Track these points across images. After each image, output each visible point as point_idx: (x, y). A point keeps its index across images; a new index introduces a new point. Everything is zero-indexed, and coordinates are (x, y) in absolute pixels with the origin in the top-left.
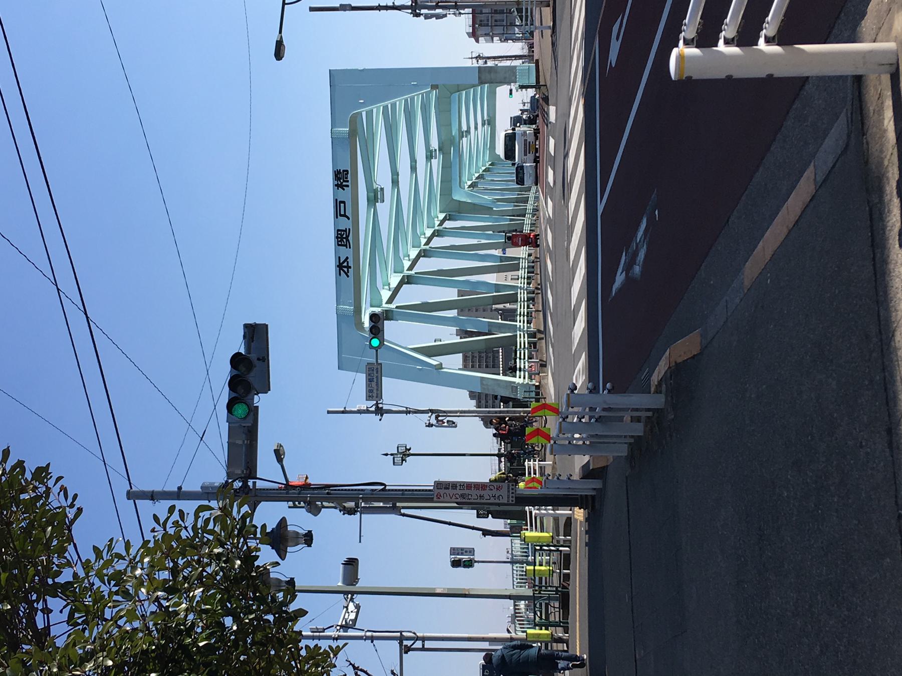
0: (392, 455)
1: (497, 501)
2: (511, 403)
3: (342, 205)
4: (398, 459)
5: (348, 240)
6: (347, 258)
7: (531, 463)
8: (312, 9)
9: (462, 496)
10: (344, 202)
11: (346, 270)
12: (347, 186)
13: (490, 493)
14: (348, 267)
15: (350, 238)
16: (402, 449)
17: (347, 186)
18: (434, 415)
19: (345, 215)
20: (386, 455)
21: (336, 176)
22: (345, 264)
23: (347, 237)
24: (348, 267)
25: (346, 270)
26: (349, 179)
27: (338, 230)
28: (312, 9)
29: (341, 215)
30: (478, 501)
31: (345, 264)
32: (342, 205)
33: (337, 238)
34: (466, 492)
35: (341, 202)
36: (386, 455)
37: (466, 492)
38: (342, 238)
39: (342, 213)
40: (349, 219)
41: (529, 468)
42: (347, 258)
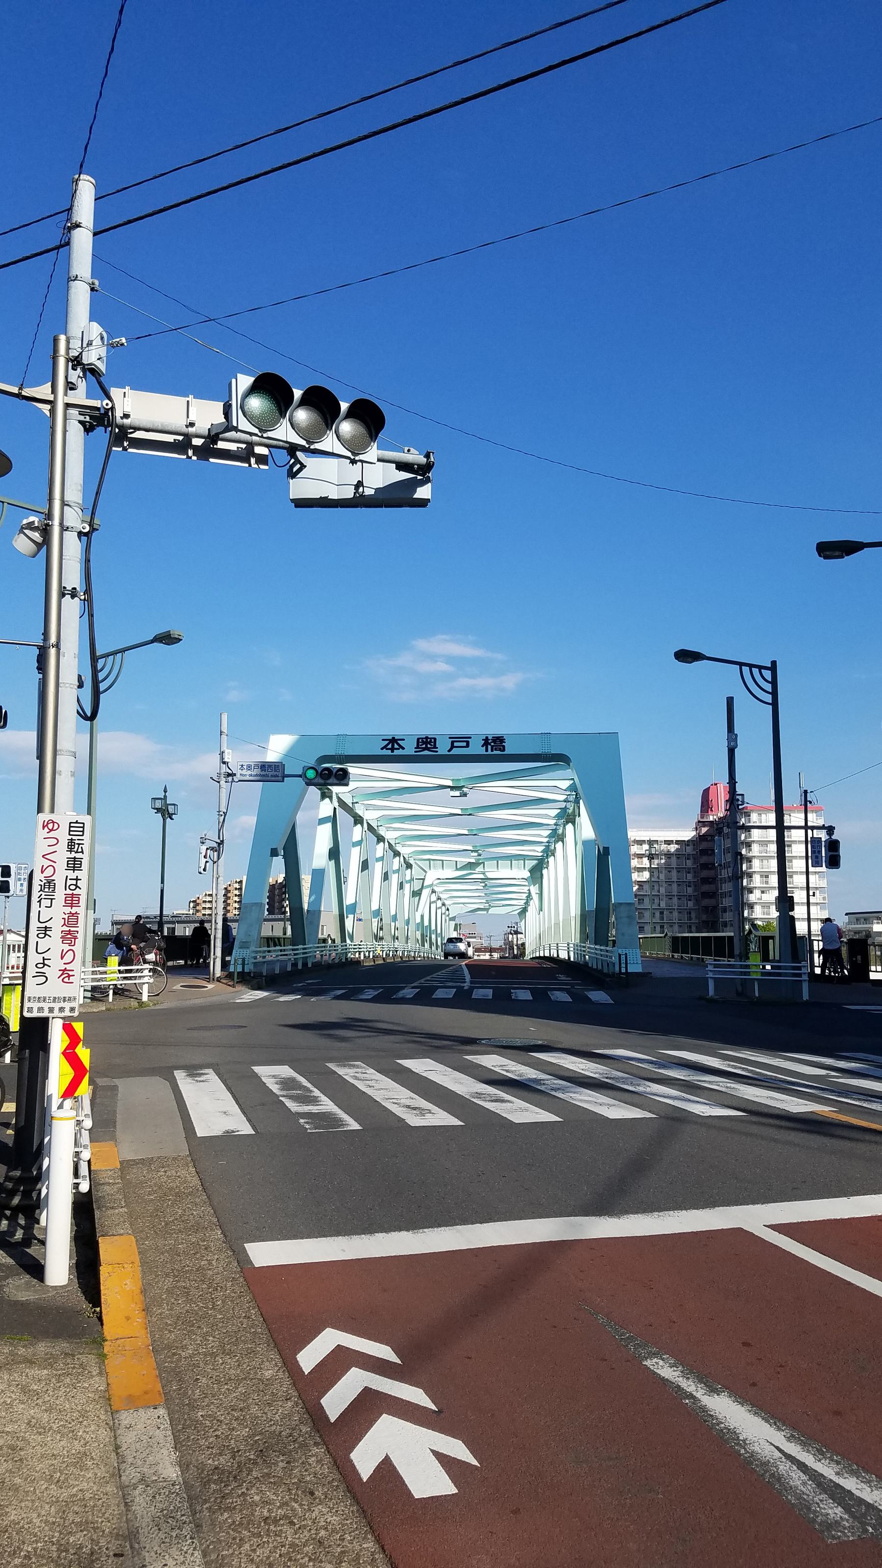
0: (165, 796)
1: (31, 970)
2: (228, 958)
3: (464, 744)
4: (158, 804)
5: (424, 749)
6: (403, 748)
7: (146, 973)
8: (730, 701)
9: (50, 884)
10: (468, 746)
11: (390, 746)
12: (487, 751)
13: (54, 957)
14: (392, 749)
15: (426, 752)
16: (171, 809)
17: (487, 751)
18: (215, 845)
19: (453, 747)
20: (165, 791)
21: (498, 738)
22: (396, 746)
23: (428, 749)
24: (392, 749)
25: (390, 746)
26: (495, 752)
27: (435, 739)
28: (730, 701)
29: (453, 743)
30: (34, 924)
31: (396, 746)
32: (464, 744)
33: (427, 738)
34: (60, 893)
35: (468, 743)
36: (165, 791)
37: (60, 893)
38: (426, 743)
39: (456, 744)
40: (449, 751)
41: (141, 971)
42: (403, 748)
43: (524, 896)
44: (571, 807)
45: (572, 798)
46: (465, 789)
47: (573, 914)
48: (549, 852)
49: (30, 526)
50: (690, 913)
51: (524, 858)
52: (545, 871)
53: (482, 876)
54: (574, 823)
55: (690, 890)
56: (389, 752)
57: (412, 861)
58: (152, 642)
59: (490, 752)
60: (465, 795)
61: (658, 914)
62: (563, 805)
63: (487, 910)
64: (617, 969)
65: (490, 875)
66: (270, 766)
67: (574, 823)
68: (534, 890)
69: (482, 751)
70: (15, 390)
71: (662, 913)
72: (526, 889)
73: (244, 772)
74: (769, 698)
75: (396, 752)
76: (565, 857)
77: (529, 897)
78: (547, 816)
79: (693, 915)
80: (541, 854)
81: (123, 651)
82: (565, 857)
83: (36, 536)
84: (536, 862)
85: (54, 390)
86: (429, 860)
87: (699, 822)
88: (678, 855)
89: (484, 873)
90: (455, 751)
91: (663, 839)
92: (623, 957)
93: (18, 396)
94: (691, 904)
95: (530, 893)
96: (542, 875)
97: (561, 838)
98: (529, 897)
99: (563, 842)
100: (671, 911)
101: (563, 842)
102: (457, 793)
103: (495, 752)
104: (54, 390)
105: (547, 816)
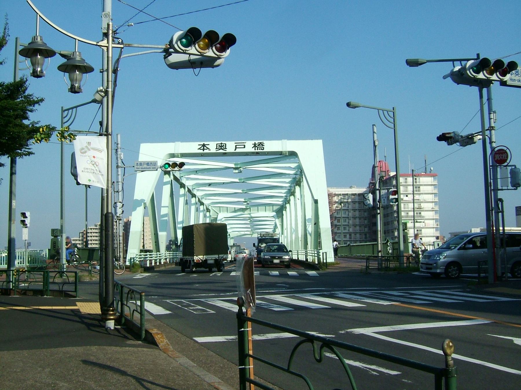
5: (220, 149)
10: (244, 147)
14: (203, 150)
19: (236, 148)
22: (205, 148)
23: (223, 149)
24: (203, 150)
25: (202, 148)
31: (205, 148)
32: (243, 146)
35: (244, 146)
39: (237, 147)
43: (272, 227)
44: (298, 177)
45: (299, 173)
46: (241, 169)
47: (300, 236)
48: (287, 201)
49: (101, 91)
50: (366, 235)
51: (273, 205)
52: (284, 212)
53: (249, 216)
54: (300, 186)
55: (366, 222)
56: (201, 151)
57: (210, 208)
58: (90, 102)
59: (256, 151)
60: (241, 172)
61: (348, 236)
62: (294, 176)
63: (252, 235)
64: (322, 260)
65: (253, 215)
66: (151, 163)
67: (300, 186)
68: (278, 222)
69: (253, 150)
70: (95, 43)
71: (350, 235)
72: (273, 223)
73: (138, 167)
74: (392, 126)
75: (206, 151)
76: (295, 204)
77: (276, 227)
78: (290, 168)
79: (368, 235)
80: (281, 203)
81: (76, 107)
82: (295, 204)
83: (103, 94)
84: (215, 64)
85: (108, 43)
86: (220, 207)
87: (371, 183)
88: (354, 202)
89: (250, 214)
90: (238, 150)
91: (351, 193)
92: (325, 254)
93: (96, 45)
94: (366, 229)
95: (276, 225)
96: (283, 215)
97: (293, 194)
98: (276, 227)
99: (294, 196)
100: (355, 234)
101: (294, 196)
102: (237, 171)
103: (259, 151)
104: (108, 43)
105: (290, 168)
